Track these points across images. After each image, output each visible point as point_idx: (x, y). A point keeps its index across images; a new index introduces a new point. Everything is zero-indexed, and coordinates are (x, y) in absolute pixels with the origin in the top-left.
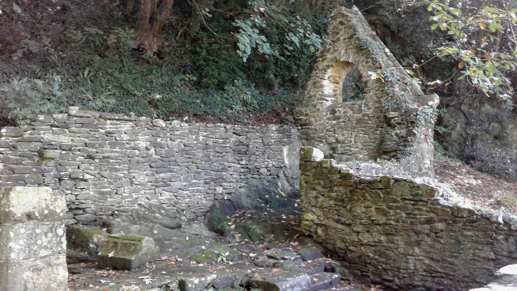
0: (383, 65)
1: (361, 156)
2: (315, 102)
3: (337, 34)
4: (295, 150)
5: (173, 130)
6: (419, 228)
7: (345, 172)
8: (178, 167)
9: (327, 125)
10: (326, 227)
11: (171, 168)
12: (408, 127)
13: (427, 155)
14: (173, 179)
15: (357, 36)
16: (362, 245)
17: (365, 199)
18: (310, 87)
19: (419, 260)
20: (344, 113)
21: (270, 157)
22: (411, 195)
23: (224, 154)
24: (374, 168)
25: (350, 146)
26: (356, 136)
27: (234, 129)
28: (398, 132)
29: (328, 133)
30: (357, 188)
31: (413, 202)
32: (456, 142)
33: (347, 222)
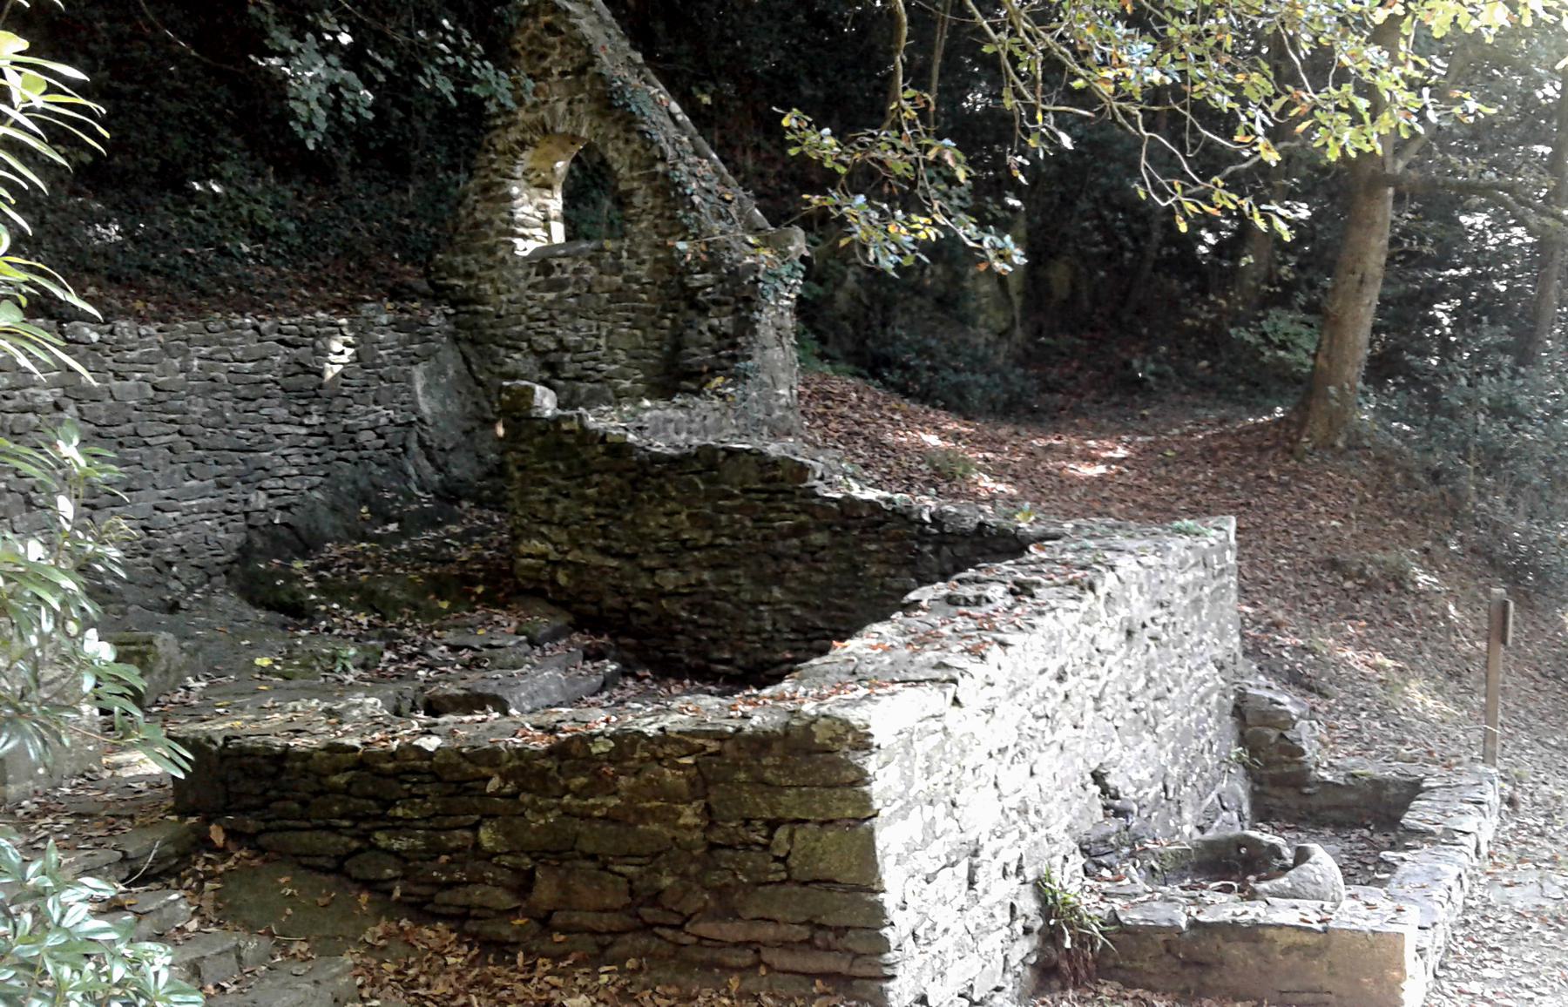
0: (670, 153)
1: (627, 384)
2: (492, 241)
3: (543, 57)
4: (443, 373)
6: (779, 546)
7: (617, 440)
8: (143, 450)
9: (530, 303)
10: (578, 569)
12: (736, 310)
13: (783, 376)
15: (596, 69)
16: (663, 595)
17: (666, 497)
19: (782, 610)
21: (381, 399)
22: (763, 481)
24: (671, 421)
25: (595, 359)
26: (610, 333)
28: (716, 322)
29: (533, 324)
30: (646, 474)
31: (764, 496)
32: (844, 318)
33: (627, 550)
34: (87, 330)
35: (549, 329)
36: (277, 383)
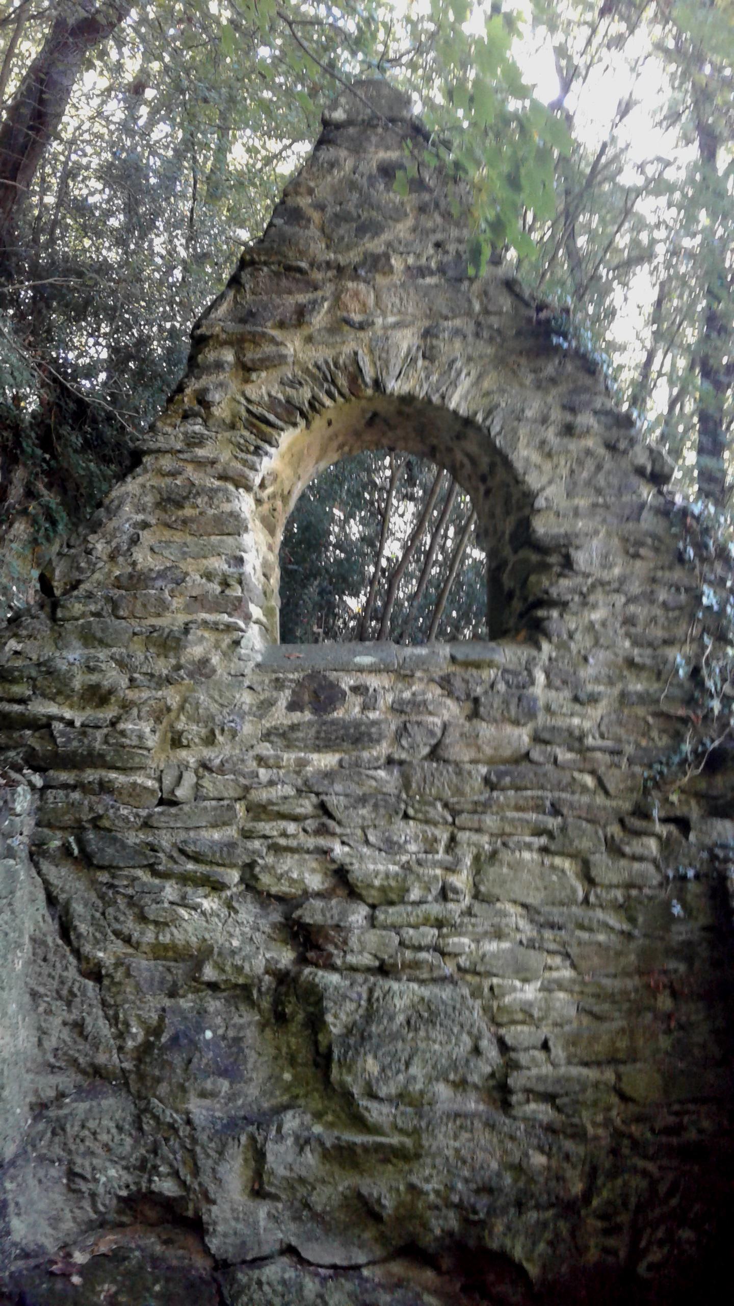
1: (530, 992)
2: (174, 620)
9: (264, 774)
18: (128, 516)
20: (398, 708)
29: (266, 827)
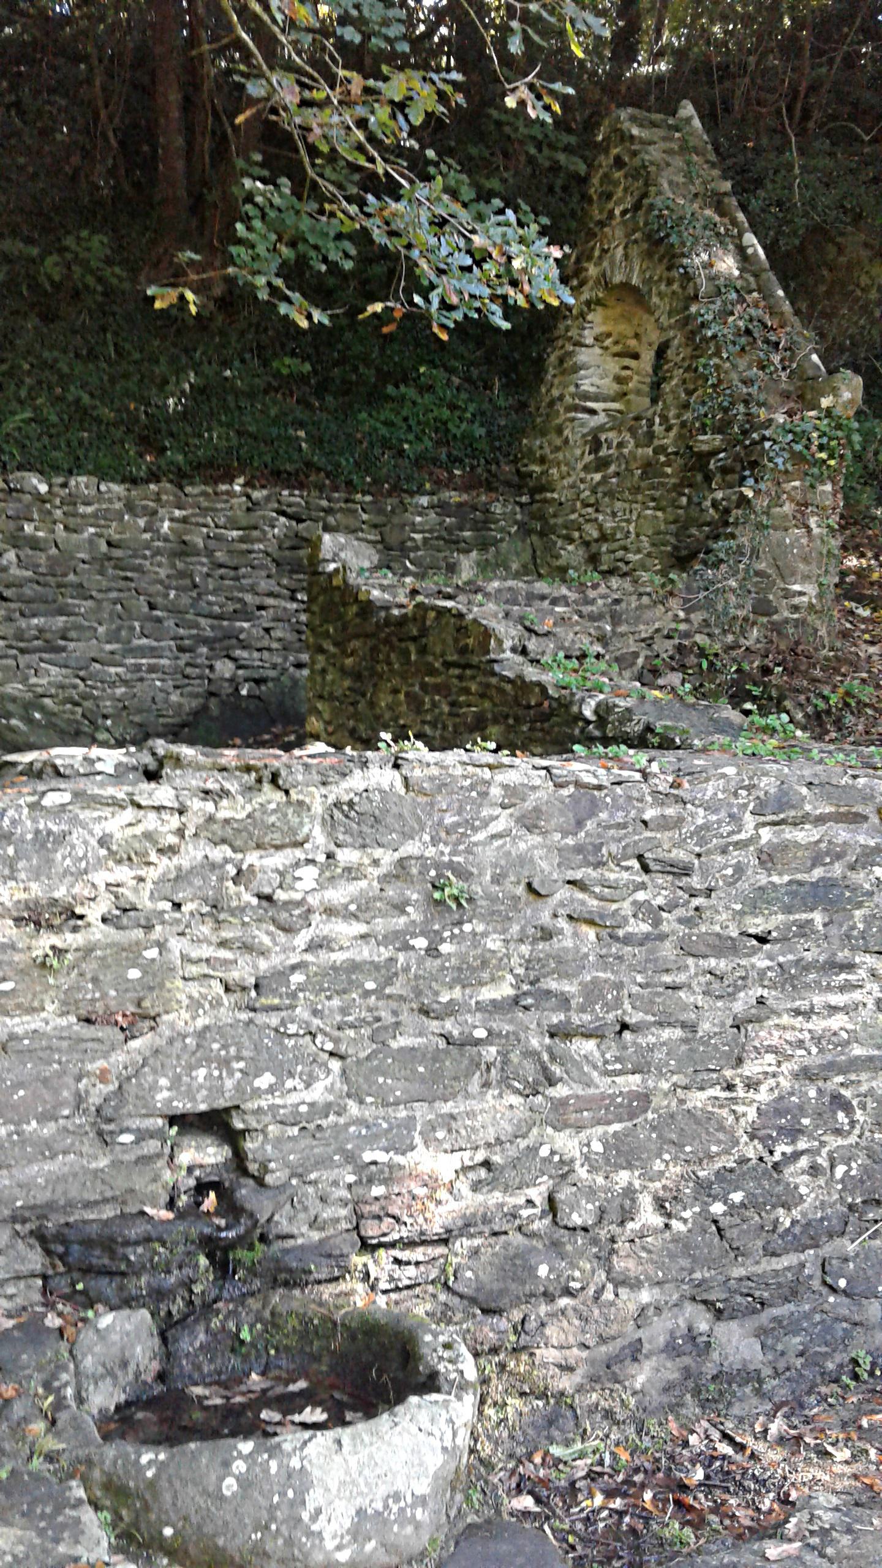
5: (72, 501)
8: (89, 603)
9: (582, 486)
11: (67, 605)
14: (73, 634)
23: (243, 570)
27: (279, 502)
28: (719, 495)
34: (35, 481)
35: (594, 516)
36: (268, 554)
